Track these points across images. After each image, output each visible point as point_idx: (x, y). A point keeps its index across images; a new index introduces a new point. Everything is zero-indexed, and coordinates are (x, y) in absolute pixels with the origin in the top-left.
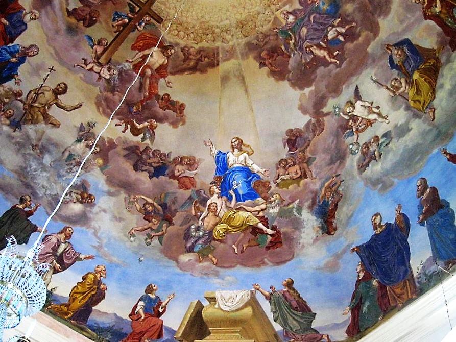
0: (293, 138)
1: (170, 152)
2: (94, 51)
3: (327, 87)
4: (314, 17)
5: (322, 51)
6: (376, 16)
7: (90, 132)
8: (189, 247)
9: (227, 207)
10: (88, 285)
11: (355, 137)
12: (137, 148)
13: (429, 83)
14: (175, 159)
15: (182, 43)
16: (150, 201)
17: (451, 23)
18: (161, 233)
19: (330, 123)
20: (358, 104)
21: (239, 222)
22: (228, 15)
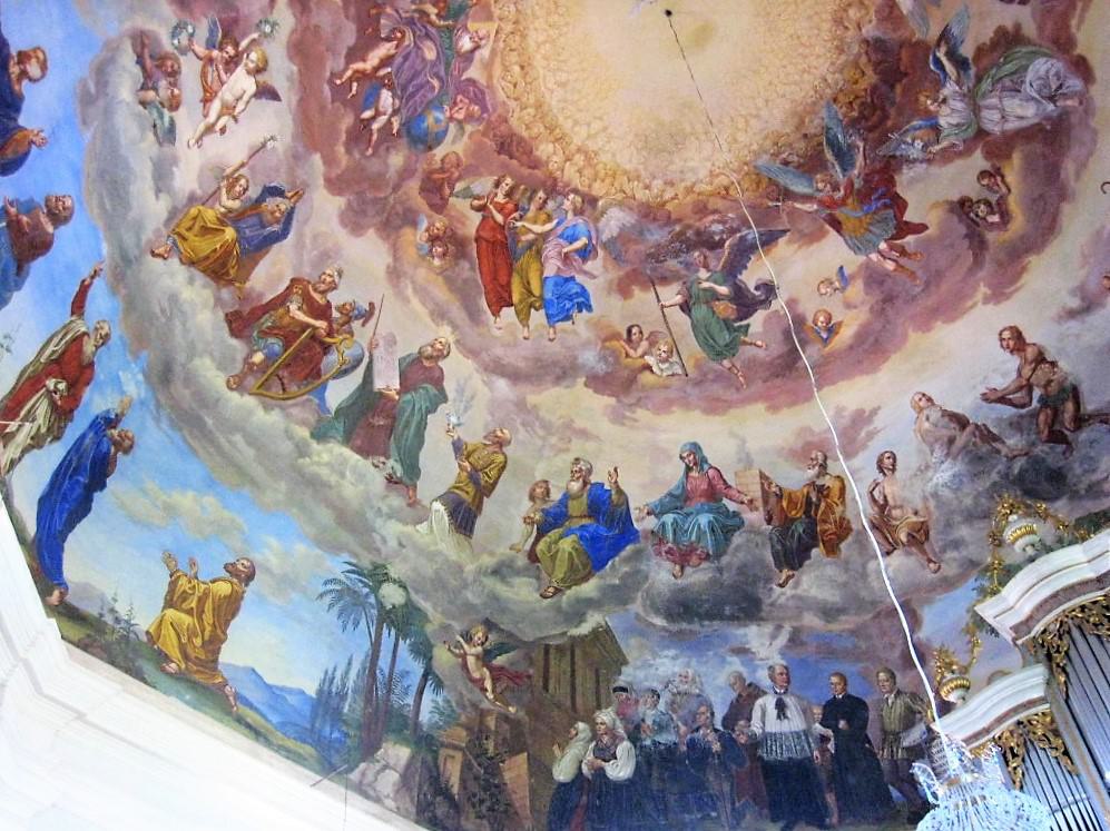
4: (433, 88)
11: (200, 49)
13: (207, 258)
17: (263, 324)
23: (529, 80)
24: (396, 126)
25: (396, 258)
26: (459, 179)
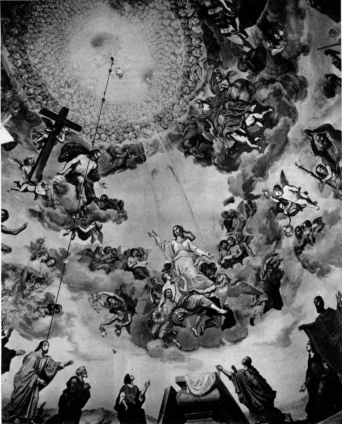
0: (229, 220)
1: (120, 247)
2: (24, 172)
3: (253, 171)
5: (243, 137)
6: (293, 101)
7: (42, 247)
8: (155, 333)
9: (181, 292)
10: (73, 390)
12: (89, 250)
14: (125, 253)
15: (106, 145)
16: (112, 294)
18: (127, 323)
19: (262, 205)
20: (286, 188)
21: (194, 306)
22: (143, 111)
23: (189, 69)
24: (254, 107)
25: (299, 54)
26: (245, 53)
